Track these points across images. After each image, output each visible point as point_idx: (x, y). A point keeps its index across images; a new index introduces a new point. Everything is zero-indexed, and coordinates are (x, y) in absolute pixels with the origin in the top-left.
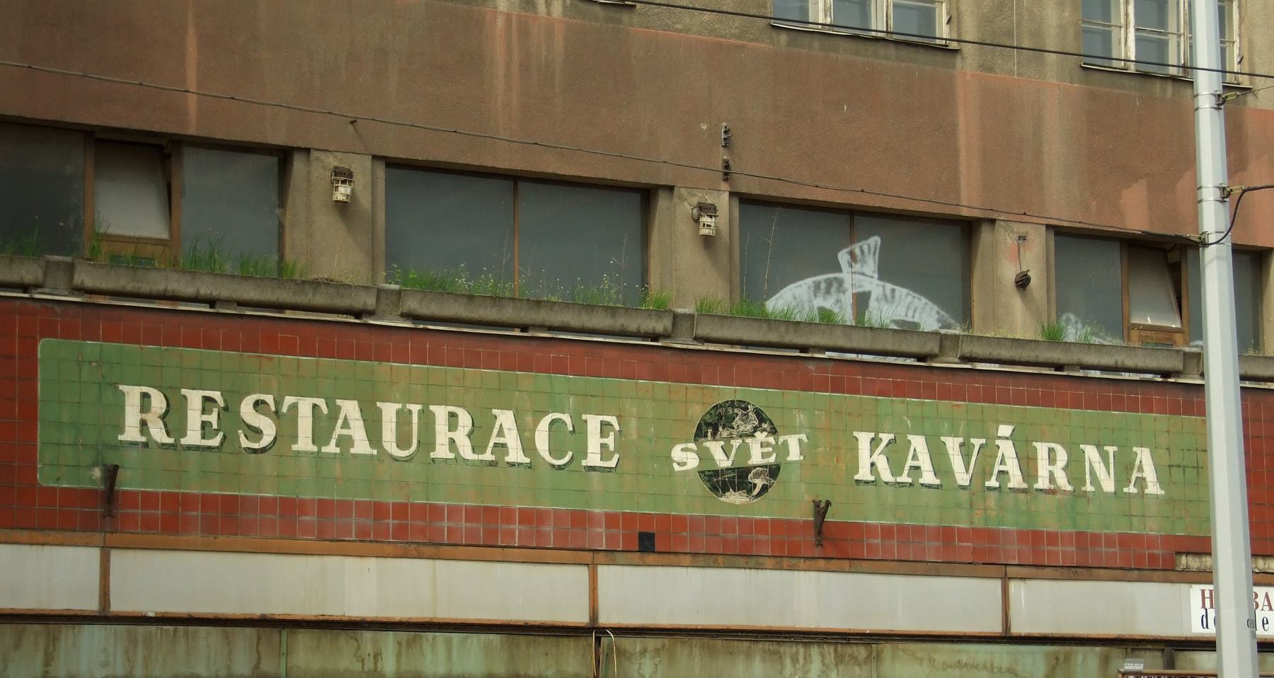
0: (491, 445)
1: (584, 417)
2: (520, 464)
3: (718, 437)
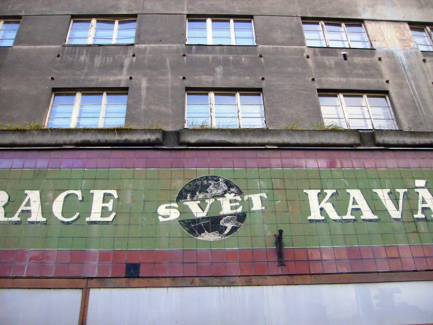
0: (19, 211)
1: (92, 191)
2: (37, 222)
3: (195, 198)
